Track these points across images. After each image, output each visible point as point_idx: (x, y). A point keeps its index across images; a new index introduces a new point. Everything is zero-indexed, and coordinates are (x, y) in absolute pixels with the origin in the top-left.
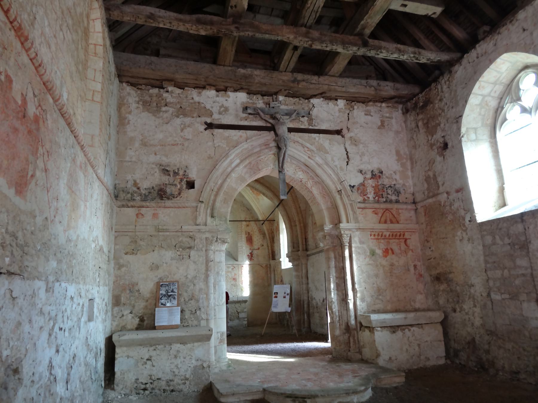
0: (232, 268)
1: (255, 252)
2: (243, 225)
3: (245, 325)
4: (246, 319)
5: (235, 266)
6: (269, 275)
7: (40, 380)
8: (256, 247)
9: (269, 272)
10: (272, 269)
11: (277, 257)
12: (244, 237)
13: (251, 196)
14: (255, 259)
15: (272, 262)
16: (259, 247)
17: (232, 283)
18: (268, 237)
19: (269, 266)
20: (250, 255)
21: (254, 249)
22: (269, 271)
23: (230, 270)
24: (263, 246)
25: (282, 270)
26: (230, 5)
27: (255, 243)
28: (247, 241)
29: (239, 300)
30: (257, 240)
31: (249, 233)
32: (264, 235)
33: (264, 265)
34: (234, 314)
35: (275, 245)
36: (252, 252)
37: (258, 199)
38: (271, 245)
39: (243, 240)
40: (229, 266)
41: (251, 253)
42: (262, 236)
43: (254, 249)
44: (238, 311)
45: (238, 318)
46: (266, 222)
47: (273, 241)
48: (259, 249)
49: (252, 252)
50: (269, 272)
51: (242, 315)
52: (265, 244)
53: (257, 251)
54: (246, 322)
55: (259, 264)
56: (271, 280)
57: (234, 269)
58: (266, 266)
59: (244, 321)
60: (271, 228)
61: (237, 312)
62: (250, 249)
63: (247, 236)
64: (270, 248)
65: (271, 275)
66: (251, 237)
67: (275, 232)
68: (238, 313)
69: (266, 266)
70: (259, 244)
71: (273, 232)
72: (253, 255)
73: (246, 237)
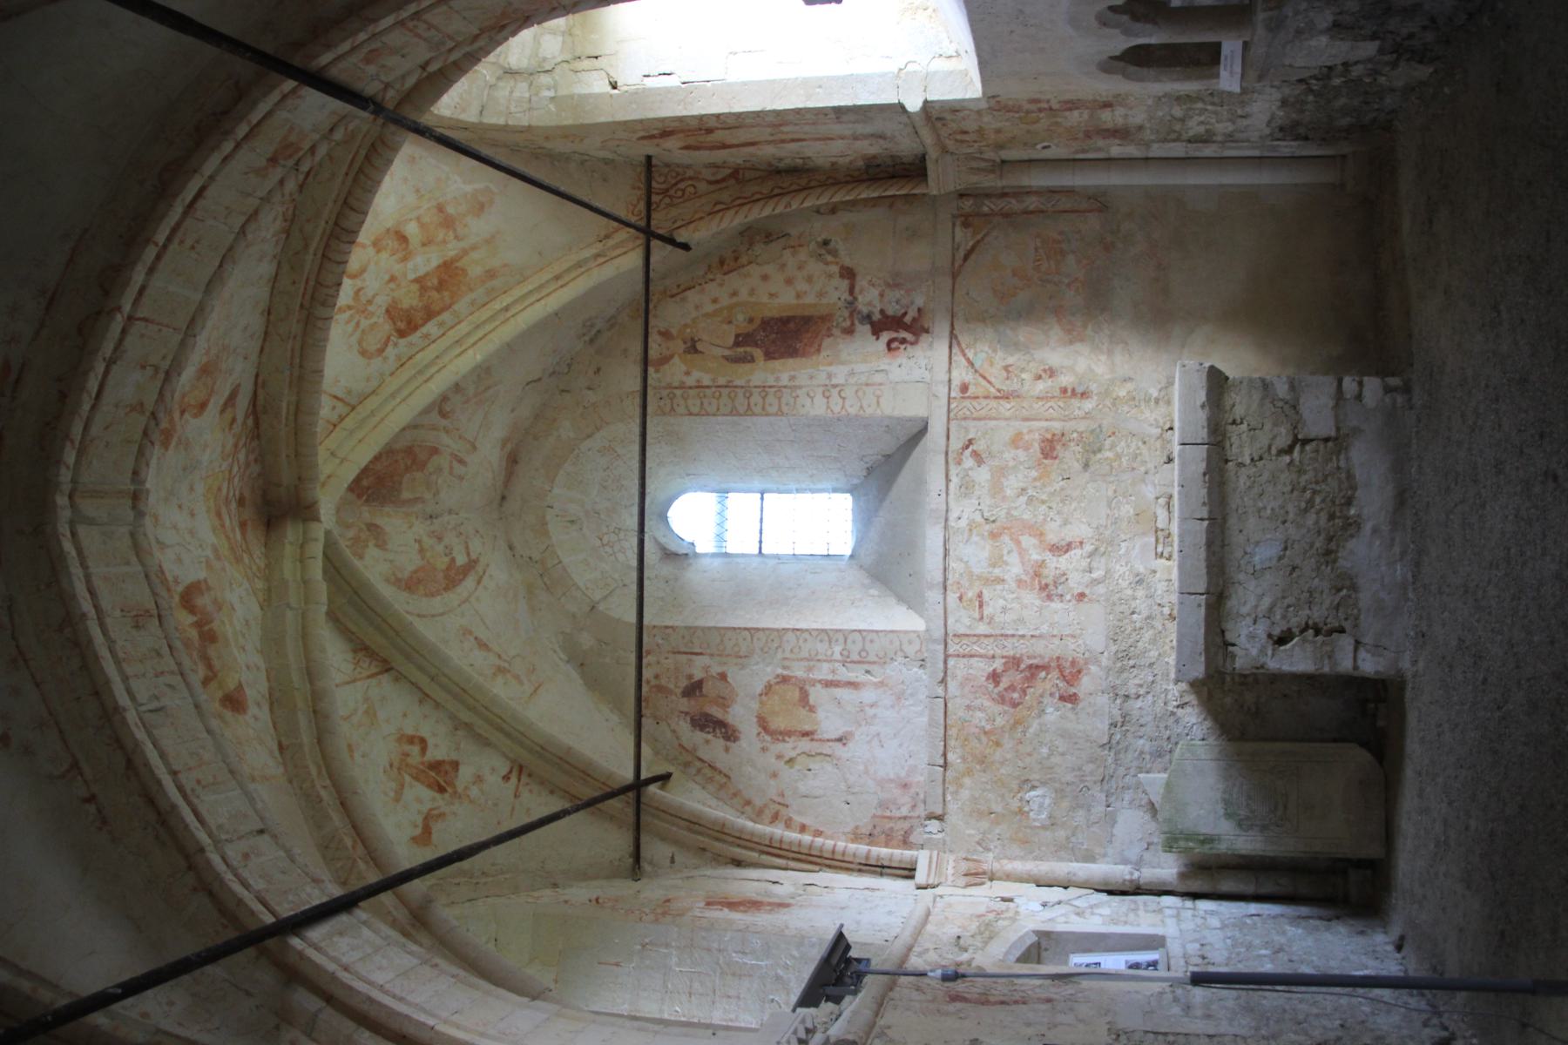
0: (969, 462)
1: (870, 298)
2: (690, 381)
3: (1388, 390)
4: (1349, 384)
5: (956, 444)
6: (1032, 203)
7: (1034, 123)
8: (836, 292)
9: (1015, 205)
10: (989, 182)
11: (906, 146)
12: (765, 373)
13: (463, 328)
14: (920, 301)
15: (943, 179)
16: (835, 269)
17: (1077, 466)
18: (767, 211)
19: (967, 205)
20: (886, 336)
21: (851, 304)
22: (1002, 204)
23: (983, 475)
24: (826, 243)
25: (989, 96)
26: (794, 302)
27: (810, 299)
28: (793, 353)
29: (1203, 434)
30: (789, 282)
31: (742, 340)
32: (758, 235)
33: (963, 237)
34: (1301, 472)
35: (820, 153)
36: (868, 318)
37: (491, 274)
38: (824, 185)
39: (785, 380)
40: (955, 480)
41: (877, 330)
42: (758, 249)
43: (851, 304)
44: (1283, 440)
45: (1337, 442)
46: (660, 222)
47: (793, 171)
48: (849, 274)
49: (868, 318)
50: (1015, 205)
51: (1318, 416)
52: (820, 228)
53: (861, 282)
54: (1372, 385)
55: (954, 276)
56: (1069, 191)
57: (979, 446)
58: (967, 221)
59: (1359, 397)
60: (702, 187)
61: (1289, 450)
62: (849, 331)
63: (758, 353)
64: (841, 196)
65: (1029, 192)
66: (766, 324)
67: (735, 157)
68: (1299, 441)
69: (966, 225)
70: (815, 267)
71: (736, 174)
72: (891, 310)
73: (769, 356)
